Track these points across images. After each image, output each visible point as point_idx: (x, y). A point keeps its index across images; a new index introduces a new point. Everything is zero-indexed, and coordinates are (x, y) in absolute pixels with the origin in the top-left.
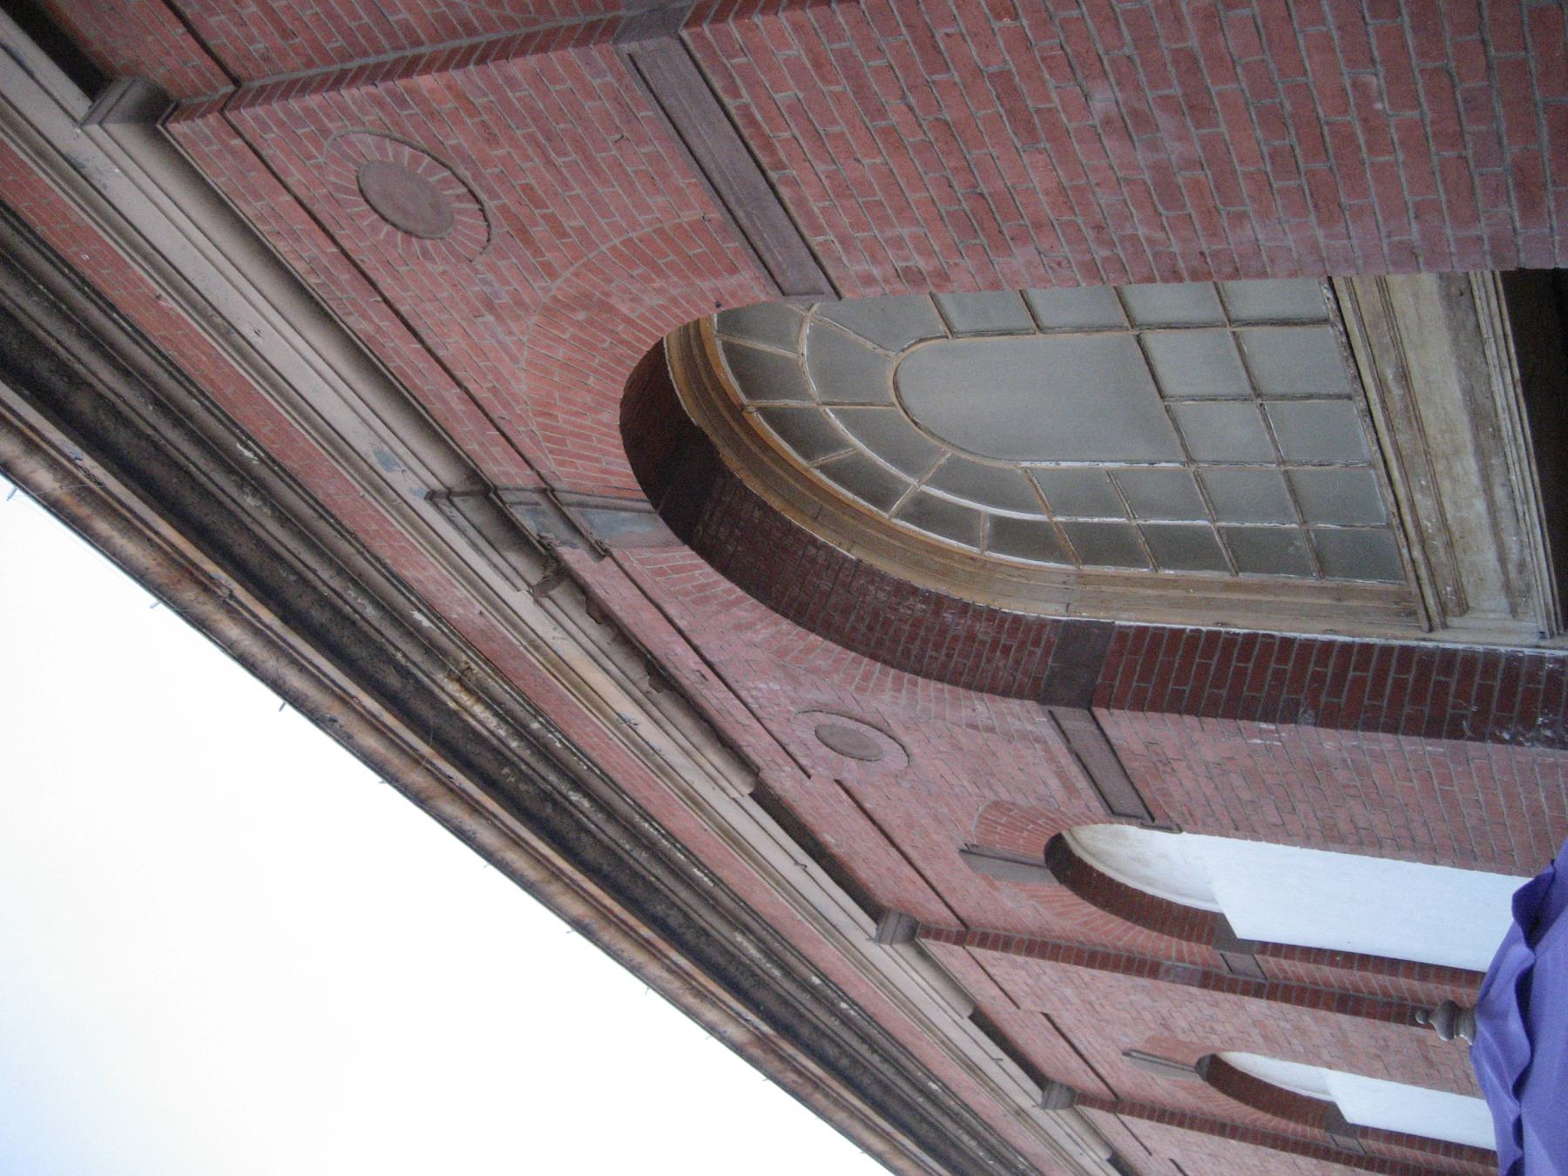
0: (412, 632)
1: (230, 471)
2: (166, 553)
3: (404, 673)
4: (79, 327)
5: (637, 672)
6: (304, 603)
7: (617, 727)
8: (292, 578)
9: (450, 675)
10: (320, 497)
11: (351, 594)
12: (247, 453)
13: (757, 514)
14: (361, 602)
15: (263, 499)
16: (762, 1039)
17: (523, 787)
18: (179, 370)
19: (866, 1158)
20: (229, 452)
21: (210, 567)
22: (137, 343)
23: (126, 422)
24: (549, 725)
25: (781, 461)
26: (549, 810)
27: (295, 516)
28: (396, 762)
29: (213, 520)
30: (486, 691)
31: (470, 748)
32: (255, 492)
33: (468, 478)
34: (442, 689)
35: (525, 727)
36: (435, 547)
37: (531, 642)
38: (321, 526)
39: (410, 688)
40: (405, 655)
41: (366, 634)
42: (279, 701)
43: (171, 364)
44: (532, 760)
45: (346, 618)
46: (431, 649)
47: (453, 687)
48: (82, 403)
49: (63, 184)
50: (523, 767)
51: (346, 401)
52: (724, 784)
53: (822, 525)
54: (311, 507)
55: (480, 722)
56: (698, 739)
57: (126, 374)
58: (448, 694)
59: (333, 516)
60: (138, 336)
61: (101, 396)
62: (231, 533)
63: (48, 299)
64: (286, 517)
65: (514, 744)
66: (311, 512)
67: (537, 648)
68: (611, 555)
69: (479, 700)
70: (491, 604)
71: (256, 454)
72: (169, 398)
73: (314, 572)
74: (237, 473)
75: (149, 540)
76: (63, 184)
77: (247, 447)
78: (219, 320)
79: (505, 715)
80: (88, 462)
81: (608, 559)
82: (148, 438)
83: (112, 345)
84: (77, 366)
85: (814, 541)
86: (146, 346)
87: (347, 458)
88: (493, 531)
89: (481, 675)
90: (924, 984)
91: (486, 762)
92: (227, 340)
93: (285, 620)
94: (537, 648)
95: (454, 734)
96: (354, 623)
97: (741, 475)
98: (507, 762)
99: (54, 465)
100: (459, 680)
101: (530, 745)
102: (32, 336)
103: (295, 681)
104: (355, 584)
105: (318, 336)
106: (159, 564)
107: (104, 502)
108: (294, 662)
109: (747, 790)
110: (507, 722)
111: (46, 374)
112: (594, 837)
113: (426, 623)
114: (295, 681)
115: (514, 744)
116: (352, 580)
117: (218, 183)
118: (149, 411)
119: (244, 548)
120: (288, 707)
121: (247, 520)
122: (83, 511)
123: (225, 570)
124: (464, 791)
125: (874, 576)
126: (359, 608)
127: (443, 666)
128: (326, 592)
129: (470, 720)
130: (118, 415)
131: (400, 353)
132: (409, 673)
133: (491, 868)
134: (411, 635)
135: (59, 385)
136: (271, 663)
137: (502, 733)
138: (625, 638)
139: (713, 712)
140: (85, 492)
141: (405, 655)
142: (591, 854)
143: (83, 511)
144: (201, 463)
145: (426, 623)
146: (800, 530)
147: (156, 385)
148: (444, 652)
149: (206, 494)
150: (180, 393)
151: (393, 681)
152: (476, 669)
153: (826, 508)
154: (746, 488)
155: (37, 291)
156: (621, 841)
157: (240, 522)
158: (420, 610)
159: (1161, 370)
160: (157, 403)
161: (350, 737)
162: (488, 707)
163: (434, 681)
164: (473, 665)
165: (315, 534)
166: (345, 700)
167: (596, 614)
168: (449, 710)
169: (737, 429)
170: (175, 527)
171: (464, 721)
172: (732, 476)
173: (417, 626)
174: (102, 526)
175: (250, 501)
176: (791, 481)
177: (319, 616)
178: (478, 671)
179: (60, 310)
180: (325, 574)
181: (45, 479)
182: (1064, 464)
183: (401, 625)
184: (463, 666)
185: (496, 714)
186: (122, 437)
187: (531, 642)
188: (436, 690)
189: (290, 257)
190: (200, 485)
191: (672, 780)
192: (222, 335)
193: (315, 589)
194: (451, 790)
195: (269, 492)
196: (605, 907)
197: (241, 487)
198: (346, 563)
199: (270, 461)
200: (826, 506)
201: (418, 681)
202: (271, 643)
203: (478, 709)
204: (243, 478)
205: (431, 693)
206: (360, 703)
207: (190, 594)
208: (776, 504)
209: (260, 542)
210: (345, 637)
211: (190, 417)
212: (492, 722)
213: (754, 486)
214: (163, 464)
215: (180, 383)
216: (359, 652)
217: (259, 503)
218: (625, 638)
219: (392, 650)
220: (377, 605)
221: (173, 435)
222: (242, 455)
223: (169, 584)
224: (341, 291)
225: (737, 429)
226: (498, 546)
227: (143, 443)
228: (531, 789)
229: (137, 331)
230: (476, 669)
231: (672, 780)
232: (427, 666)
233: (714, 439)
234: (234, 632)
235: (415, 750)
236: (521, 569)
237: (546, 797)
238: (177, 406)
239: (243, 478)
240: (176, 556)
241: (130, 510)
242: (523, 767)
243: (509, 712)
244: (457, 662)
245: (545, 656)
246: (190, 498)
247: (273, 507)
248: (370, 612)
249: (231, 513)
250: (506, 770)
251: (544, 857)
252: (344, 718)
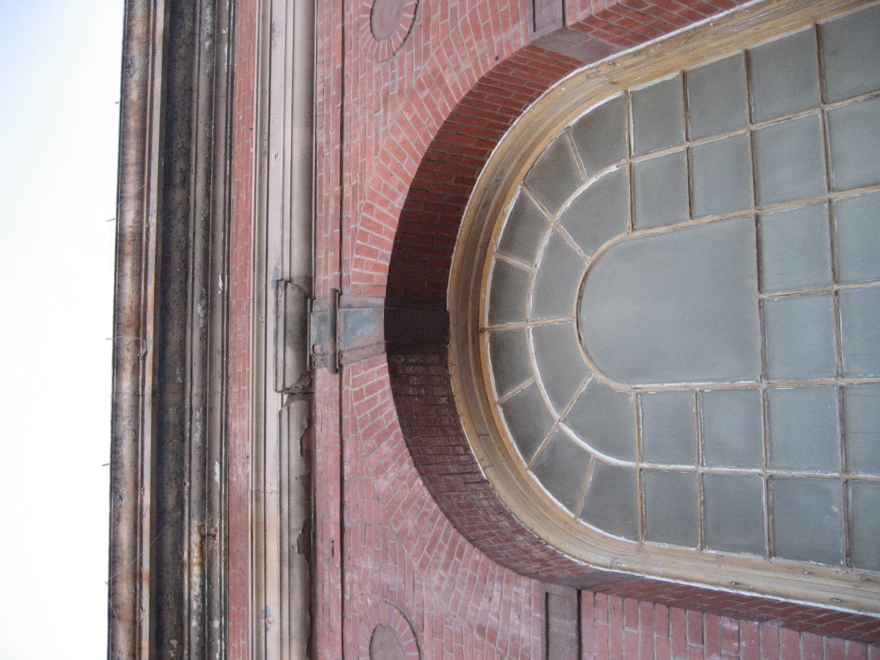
1: (205, 285)
2: (139, 304)
3: (180, 504)
4: (210, 157)
5: (297, 524)
6: (171, 398)
7: (258, 617)
8: (179, 379)
9: (201, 527)
10: (231, 338)
11: (197, 415)
12: (220, 284)
13: (444, 400)
14: (197, 425)
15: (206, 315)
16: (139, 235)
18: (230, 211)
20: (213, 275)
21: (150, 328)
22: (225, 183)
23: (186, 223)
24: (224, 628)
25: (483, 387)
28: (125, 566)
30: (210, 566)
31: (170, 599)
32: (206, 308)
34: (190, 534)
35: (211, 619)
36: (258, 404)
37: (258, 491)
38: (218, 358)
39: (174, 515)
40: (190, 488)
41: (183, 453)
43: (230, 204)
45: (183, 434)
46: (206, 497)
47: (196, 538)
48: (178, 196)
50: (186, 652)
52: (286, 644)
53: (480, 441)
54: (223, 347)
55: (189, 583)
56: (296, 627)
57: (208, 194)
60: (228, 181)
61: (188, 201)
62: (176, 322)
63: (210, 134)
64: (207, 336)
65: (194, 623)
67: (258, 499)
69: (202, 565)
70: (258, 457)
71: (223, 287)
72: (213, 252)
74: (207, 291)
78: (266, 144)
79: (206, 595)
80: (153, 220)
81: (338, 376)
82: (187, 238)
83: (215, 177)
85: (467, 448)
86: (227, 187)
87: (258, 589)
89: (217, 548)
90: (288, 157)
91: (170, 619)
92: (261, 158)
93: (154, 394)
94: (258, 499)
95: (169, 577)
96: (183, 441)
97: (452, 370)
98: (180, 637)
99: (139, 213)
100: (203, 537)
101: (202, 635)
102: (189, 150)
103: (126, 449)
105: (299, 133)
106: (131, 307)
107: (141, 251)
110: (203, 601)
111: (178, 169)
113: (217, 478)
114: (126, 449)
115: (194, 623)
116: (205, 408)
117: (319, 23)
118: (200, 219)
122: (129, 248)
124: (140, 628)
125: (490, 493)
126: (194, 430)
127: (202, 518)
130: (186, 215)
131: (327, 170)
132: (182, 506)
134: (204, 476)
135: (178, 179)
136: (126, 424)
138: (308, 482)
139: (320, 603)
140: (139, 235)
141: (190, 488)
143: (129, 248)
144: (197, 267)
145: (217, 478)
146: (463, 436)
147: (214, 213)
148: (211, 511)
149: (184, 292)
150: (220, 225)
151: (171, 501)
153: (489, 435)
154: (449, 382)
155: (210, 127)
159: (767, 258)
160: (206, 220)
161: (118, 519)
162: (202, 575)
164: (218, 538)
165: (212, 266)
166: (137, 486)
167: (305, 447)
168: (181, 557)
169: (470, 341)
170: (155, 289)
172: (447, 367)
173: (211, 472)
175: (199, 310)
177: (172, 416)
178: (218, 544)
179: (210, 142)
180: (196, 390)
181: (130, 217)
182: (666, 385)
184: (212, 531)
185: (202, 587)
186: (178, 227)
187: (258, 491)
189: (319, 80)
192: (261, 152)
193: (184, 398)
195: (211, 318)
196: (140, 644)
197: (202, 298)
200: (491, 436)
201: (182, 518)
202: (137, 408)
203: (196, 570)
205: (182, 534)
207: (128, 339)
208: (461, 407)
209: (183, 343)
210: (172, 442)
211: (213, 242)
212: (196, 591)
213: (455, 385)
215: (225, 219)
216: (170, 461)
217: (202, 315)
218: (308, 482)
219: (186, 480)
221: (199, 241)
222: (217, 283)
225: (470, 341)
227: (183, 239)
229: (230, 177)
230: (217, 542)
232: (195, 508)
234: (127, 384)
235: (141, 564)
236: (288, 367)
239: (207, 295)
240: (142, 309)
241: (146, 265)
242: (186, 652)
243: (210, 596)
244: (211, 525)
245: (257, 508)
246: (175, 286)
247: (206, 326)
248: (197, 437)
252: (126, 490)
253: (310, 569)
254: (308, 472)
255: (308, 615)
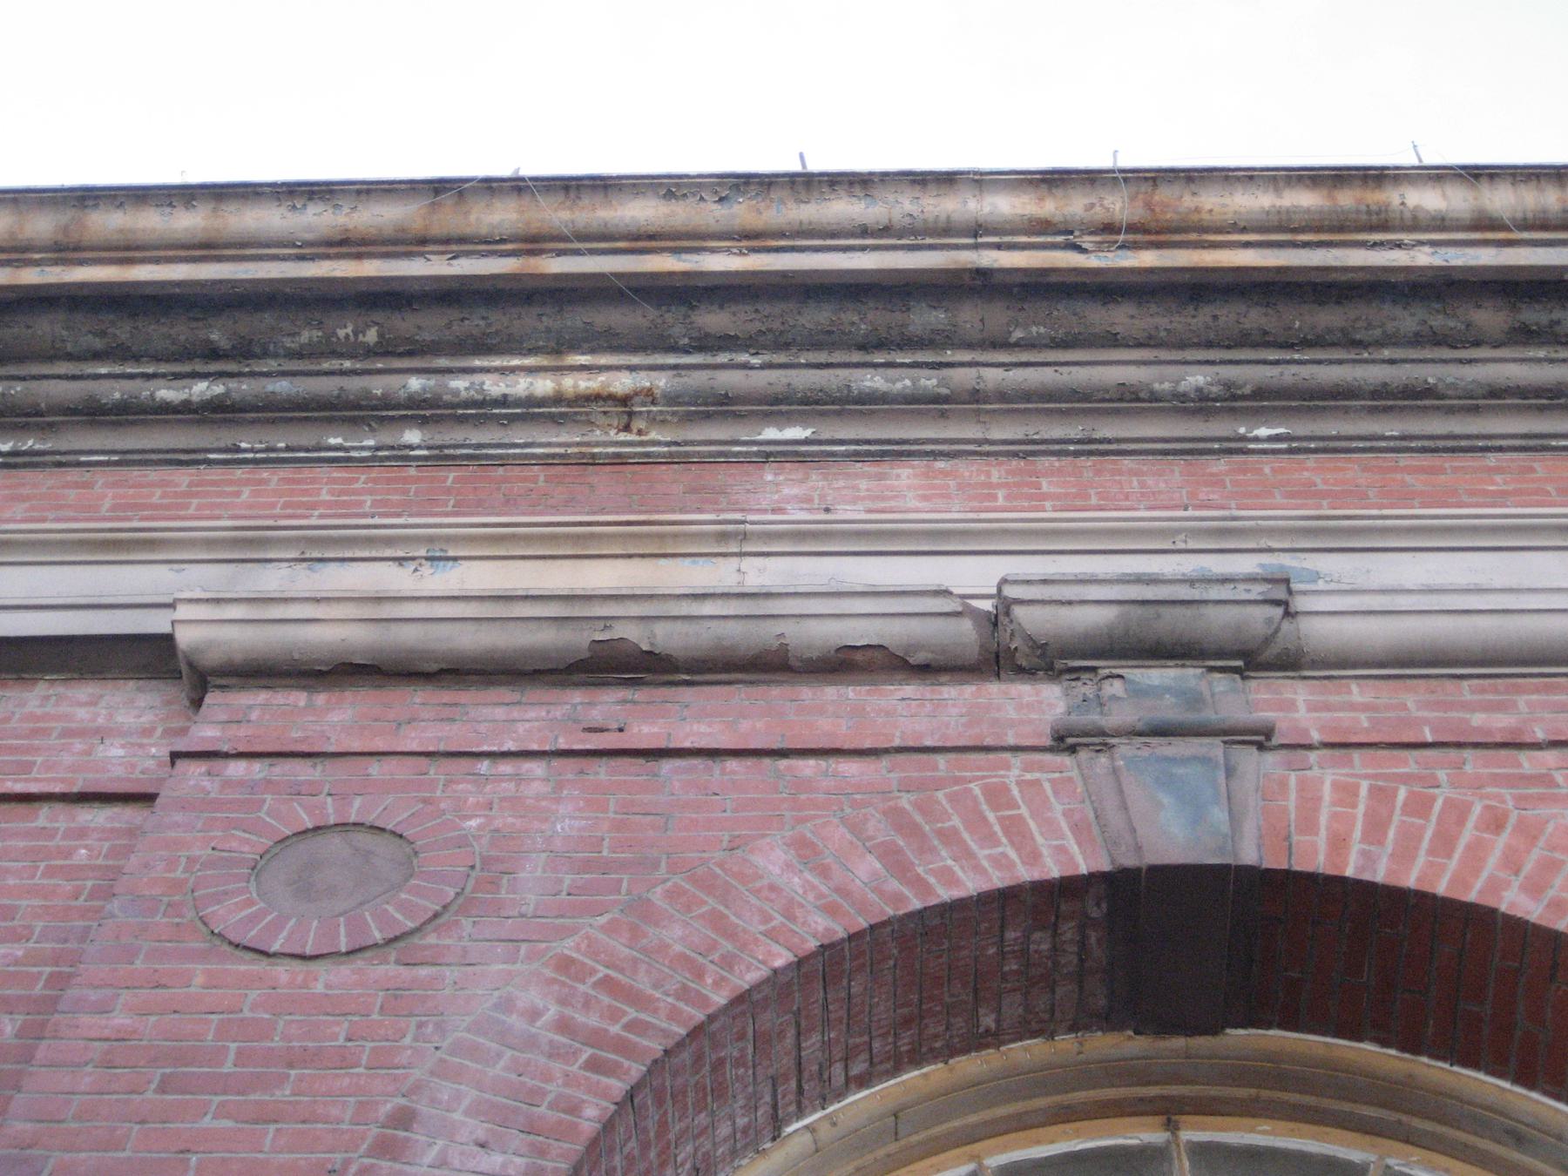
0: (778, 406)
1: (1260, 393)
3: (705, 343)
5: (667, 638)
6: (969, 316)
7: (430, 540)
8: (1018, 334)
9: (649, 395)
11: (929, 381)
12: (1263, 432)
13: (988, 1021)
14: (903, 382)
15: (1182, 397)
17: (306, 336)
18: (1453, 450)
19: (501, 168)
21: (1148, 259)
24: (401, 456)
26: (217, 336)
27: (1117, 412)
28: (556, 215)
29: (1200, 318)
30: (556, 420)
31: (476, 322)
32: (1202, 396)
33: (1300, 653)
34: (632, 368)
35: (423, 422)
38: (1074, 430)
39: (677, 330)
40: (746, 366)
41: (832, 346)
42: (815, 166)
44: (354, 385)
45: (881, 345)
46: (722, 406)
47: (622, 383)
48: (1490, 317)
49: (1020, 525)
51: (286, 600)
53: (881, 1117)
56: (408, 636)
58: (618, 368)
59: (1077, 454)
61: (1477, 344)
62: (1162, 322)
64: (1130, 400)
65: (415, 383)
66: (1109, 434)
67: (723, 537)
68: (1050, 750)
69: (558, 399)
71: (1257, 439)
73: (1007, 366)
75: (1244, 230)
76: (1064, 525)
77: (1271, 439)
79: (484, 410)
80: (1423, 258)
81: (1047, 741)
82: (1380, 344)
83: (1541, 409)
84: (1541, 353)
88: (1173, 622)
89: (598, 435)
94: (723, 537)
95: (528, 320)
96: (862, 347)
97: (1066, 1043)
98: (384, 349)
99: (1440, 223)
101: (386, 403)
103: (842, 209)
104: (937, 399)
106: (1197, 210)
107: (1341, 229)
108: (886, 231)
109: (186, 638)
112: (70, 357)
113: (771, 433)
115: (415, 383)
116: (946, 400)
118: (1431, 375)
119: (1122, 317)
120: (796, 167)
121: (1164, 355)
122: (1347, 199)
123: (1132, 270)
124: (408, 255)
126: (891, 372)
127: (672, 399)
128: (950, 355)
129: (529, 361)
132: (701, 349)
133: (505, 171)
135: (1534, 315)
137: (459, 384)
140: (1380, 223)
141: (746, 366)
142: (46, 327)
143: (1347, 199)
144: (1305, 372)
145: (771, 433)
146: (897, 1070)
147: (1451, 411)
148: (689, 418)
151: (714, 320)
152: (613, 435)
156: (19, 387)
157: (1160, 345)
158: (806, 442)
160: (1429, 392)
161: (670, 195)
162: (531, 401)
163: (661, 368)
164: (623, 437)
166: (752, 239)
167: (858, 657)
168: (575, 347)
171: (532, 351)
172: (1073, 1028)
173: (788, 419)
174: (1305, 200)
175: (1196, 378)
176: (973, 1119)
177: (925, 318)
178: (606, 437)
181: (1428, 200)
183: (805, 401)
184: (639, 424)
185: (504, 401)
186: (1408, 320)
188: (635, 360)
190: (1255, 345)
191: (210, 544)
194: (423, 241)
195: (1177, 410)
196: (143, 261)
197: (1228, 385)
198: (978, 412)
199: (1235, 448)
200: (893, 1147)
201: (674, 349)
202: (943, 232)
203: (544, 386)
204: (1234, 398)
206: (728, 250)
208: (970, 1065)
211: (1372, 411)
212: (494, 386)
213: (1026, 1052)
214: (1330, 331)
217: (1183, 387)
218: (771, 666)
220: (166, 408)
223: (1158, 196)
224: (1416, 706)
226: (1138, 611)
228: (288, 343)
230: (613, 435)
231: (210, 544)
232: (698, 379)
233: (1178, 1042)
237: (244, 351)
238: (1402, 409)
239: (1234, 398)
241: (1306, 245)
242: (347, 364)
244: (653, 420)
246: (1255, 317)
247: (1155, 397)
248: (873, 381)
249: (1182, 345)
250: (371, 336)
251: (131, 261)
253: (551, 671)
254: (793, 662)
255: (435, 667)
